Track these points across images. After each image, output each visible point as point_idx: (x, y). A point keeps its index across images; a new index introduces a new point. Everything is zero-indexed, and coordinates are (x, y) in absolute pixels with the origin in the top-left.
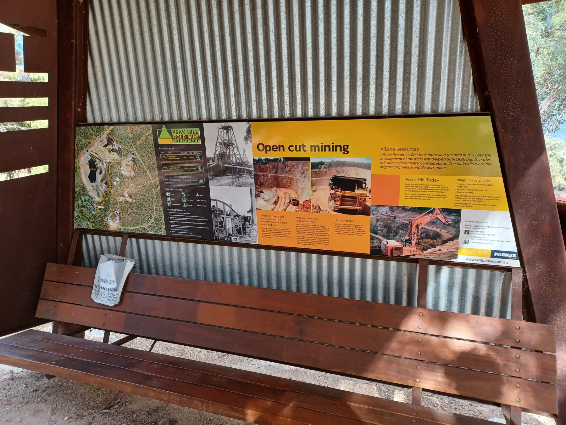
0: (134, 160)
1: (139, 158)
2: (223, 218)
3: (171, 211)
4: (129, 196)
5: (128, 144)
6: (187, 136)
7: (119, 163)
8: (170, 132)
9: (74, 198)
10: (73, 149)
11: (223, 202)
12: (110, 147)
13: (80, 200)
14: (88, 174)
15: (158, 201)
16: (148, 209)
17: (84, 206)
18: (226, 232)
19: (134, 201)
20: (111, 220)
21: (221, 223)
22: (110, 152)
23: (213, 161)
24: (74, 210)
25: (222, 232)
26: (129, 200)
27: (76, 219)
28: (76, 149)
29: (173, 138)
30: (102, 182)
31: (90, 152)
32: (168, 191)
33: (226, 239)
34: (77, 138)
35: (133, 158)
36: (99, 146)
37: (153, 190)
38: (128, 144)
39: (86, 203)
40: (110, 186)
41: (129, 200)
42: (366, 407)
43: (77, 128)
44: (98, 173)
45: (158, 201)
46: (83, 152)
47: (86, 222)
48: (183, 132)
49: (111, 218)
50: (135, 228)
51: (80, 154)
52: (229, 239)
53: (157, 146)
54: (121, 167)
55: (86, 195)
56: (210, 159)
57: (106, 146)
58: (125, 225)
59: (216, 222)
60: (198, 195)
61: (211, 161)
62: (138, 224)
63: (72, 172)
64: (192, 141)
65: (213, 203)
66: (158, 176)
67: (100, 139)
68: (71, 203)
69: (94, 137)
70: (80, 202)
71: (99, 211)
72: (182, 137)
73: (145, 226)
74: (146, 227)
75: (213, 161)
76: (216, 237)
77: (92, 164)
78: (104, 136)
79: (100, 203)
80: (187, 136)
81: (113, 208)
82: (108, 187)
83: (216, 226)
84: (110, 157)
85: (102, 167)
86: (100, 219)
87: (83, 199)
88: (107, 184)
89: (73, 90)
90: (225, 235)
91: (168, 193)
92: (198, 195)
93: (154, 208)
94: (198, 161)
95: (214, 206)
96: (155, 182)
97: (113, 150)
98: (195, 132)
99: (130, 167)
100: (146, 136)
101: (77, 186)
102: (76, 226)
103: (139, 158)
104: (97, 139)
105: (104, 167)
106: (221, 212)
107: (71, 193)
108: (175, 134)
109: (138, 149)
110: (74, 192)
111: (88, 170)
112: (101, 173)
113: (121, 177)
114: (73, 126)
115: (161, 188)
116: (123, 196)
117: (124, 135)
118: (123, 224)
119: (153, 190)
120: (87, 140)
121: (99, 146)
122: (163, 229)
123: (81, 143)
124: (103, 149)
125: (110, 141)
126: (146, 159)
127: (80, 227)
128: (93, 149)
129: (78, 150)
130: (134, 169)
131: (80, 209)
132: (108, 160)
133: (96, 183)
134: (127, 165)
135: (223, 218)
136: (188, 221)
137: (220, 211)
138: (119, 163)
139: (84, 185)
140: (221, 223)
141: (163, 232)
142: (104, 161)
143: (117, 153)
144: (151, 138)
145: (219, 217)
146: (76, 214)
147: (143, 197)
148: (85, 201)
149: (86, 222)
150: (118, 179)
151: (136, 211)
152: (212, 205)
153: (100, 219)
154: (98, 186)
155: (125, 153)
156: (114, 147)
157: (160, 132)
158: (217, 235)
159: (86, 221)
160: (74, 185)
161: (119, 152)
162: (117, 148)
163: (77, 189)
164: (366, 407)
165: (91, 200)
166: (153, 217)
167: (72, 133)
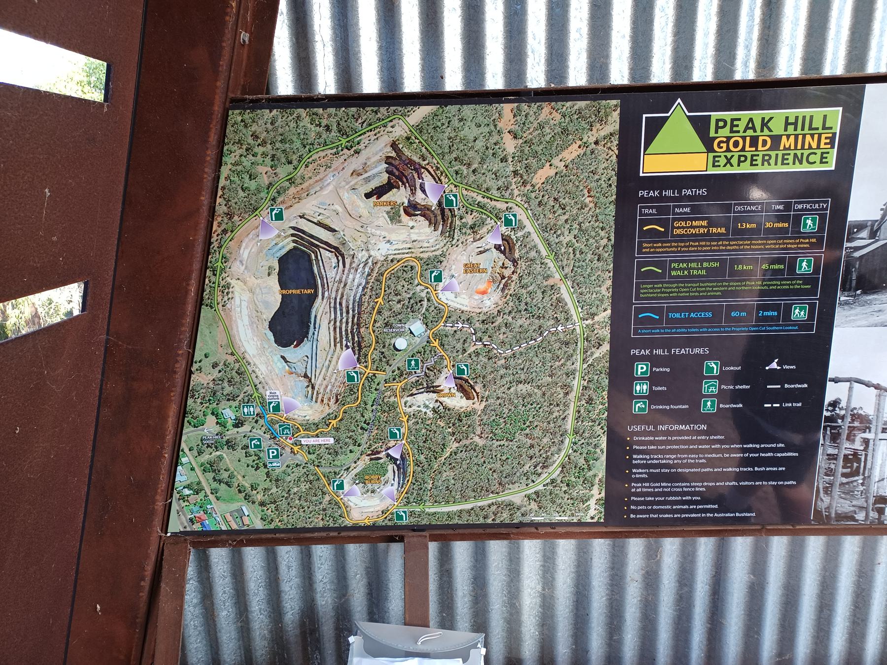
0: (507, 247)
1: (536, 239)
2: (866, 442)
3: (645, 433)
4: (461, 389)
5: (490, 182)
6: (776, 140)
7: (437, 261)
8: (701, 126)
9: (183, 412)
10: (205, 210)
11: (877, 387)
12: (400, 196)
13: (211, 420)
14: (269, 314)
15: (590, 401)
16: (537, 433)
17: (231, 445)
18: (865, 493)
19: (479, 407)
20: (358, 489)
21: (853, 459)
22: (394, 217)
23: (873, 235)
24: (175, 462)
25: (849, 493)
26: (458, 402)
27: (183, 498)
28: (221, 209)
29: (710, 149)
30: (337, 342)
31: (291, 219)
32: (642, 359)
33: (861, 516)
34: (229, 160)
35: (506, 239)
36: (346, 196)
37: (579, 357)
38: (490, 182)
39: (246, 428)
40: (373, 354)
41: (458, 402)
42: (738, 455)
43: (235, 116)
44: (320, 308)
45: (590, 401)
46: (253, 222)
47: (235, 506)
48: (764, 124)
49: (361, 478)
50: (468, 506)
51: (238, 233)
52: (873, 515)
53: (629, 182)
54: (438, 279)
55: (249, 400)
56: (861, 226)
57: (379, 192)
58: (420, 501)
59: (832, 457)
60: (774, 365)
61: (865, 234)
62: (482, 490)
63: (190, 308)
64: (798, 159)
65: (832, 392)
66: (607, 304)
67: (356, 163)
68: (169, 438)
69: (319, 154)
70: (210, 427)
71: (302, 457)
72: (754, 141)
73: (516, 495)
74: (517, 499)
75: (873, 235)
76: (818, 513)
77: (297, 269)
78: (375, 151)
79: (312, 428)
80: (776, 140)
81: (377, 439)
82: (361, 358)
83: (830, 472)
84: (391, 237)
85: (340, 281)
86: (304, 487)
87: (229, 414)
88: (359, 348)
89: (675, 427)
90: (861, 502)
91: (641, 368)
92: (774, 365)
93: (569, 425)
94: (809, 236)
95: (834, 404)
96: (591, 328)
97: (412, 209)
98: (818, 123)
99: (486, 277)
100: (586, 145)
101: (207, 364)
102: (176, 525)
103: (536, 239)
104: (337, 163)
105: (356, 280)
106: (865, 423)
107: (175, 395)
108: (725, 132)
109: (538, 203)
110: (186, 391)
111: (272, 296)
112: (336, 306)
113: (435, 315)
114: (217, 108)
115: (613, 352)
116: (432, 389)
117: (480, 144)
118: (414, 494)
119: (579, 357)
120: (283, 171)
121: (346, 196)
122: (592, 503)
123: (253, 185)
124: (364, 207)
125: (400, 171)
126: (567, 238)
127: (197, 527)
128: (309, 206)
129: (230, 215)
130: (502, 282)
131: (205, 457)
132: (381, 251)
133: (306, 348)
134: (471, 268)
135: (866, 442)
136: (711, 463)
137: (855, 417)
138: (437, 261)
139: (241, 359)
140: (853, 459)
141: (592, 512)
142: (362, 256)
143: (433, 223)
144: (609, 156)
145: (850, 438)
146: (182, 477)
147: (523, 388)
148: (238, 423)
149: (235, 506)
150: (417, 327)
151: (481, 442)
152: (829, 398)
153: (304, 487)
154: (314, 356)
155: (469, 220)
156: (419, 197)
157: (655, 127)
158: (822, 506)
159: (231, 500)
160: (191, 360)
161: (441, 216)
162: (433, 201)
163: (201, 379)
164: (738, 455)
165: (270, 416)
166: (559, 459)
167: (213, 138)
